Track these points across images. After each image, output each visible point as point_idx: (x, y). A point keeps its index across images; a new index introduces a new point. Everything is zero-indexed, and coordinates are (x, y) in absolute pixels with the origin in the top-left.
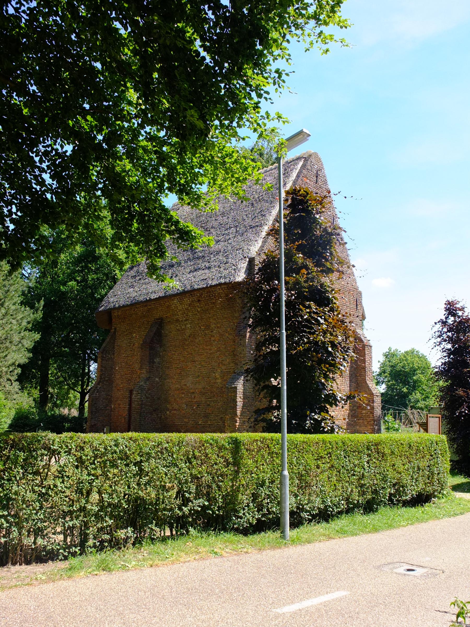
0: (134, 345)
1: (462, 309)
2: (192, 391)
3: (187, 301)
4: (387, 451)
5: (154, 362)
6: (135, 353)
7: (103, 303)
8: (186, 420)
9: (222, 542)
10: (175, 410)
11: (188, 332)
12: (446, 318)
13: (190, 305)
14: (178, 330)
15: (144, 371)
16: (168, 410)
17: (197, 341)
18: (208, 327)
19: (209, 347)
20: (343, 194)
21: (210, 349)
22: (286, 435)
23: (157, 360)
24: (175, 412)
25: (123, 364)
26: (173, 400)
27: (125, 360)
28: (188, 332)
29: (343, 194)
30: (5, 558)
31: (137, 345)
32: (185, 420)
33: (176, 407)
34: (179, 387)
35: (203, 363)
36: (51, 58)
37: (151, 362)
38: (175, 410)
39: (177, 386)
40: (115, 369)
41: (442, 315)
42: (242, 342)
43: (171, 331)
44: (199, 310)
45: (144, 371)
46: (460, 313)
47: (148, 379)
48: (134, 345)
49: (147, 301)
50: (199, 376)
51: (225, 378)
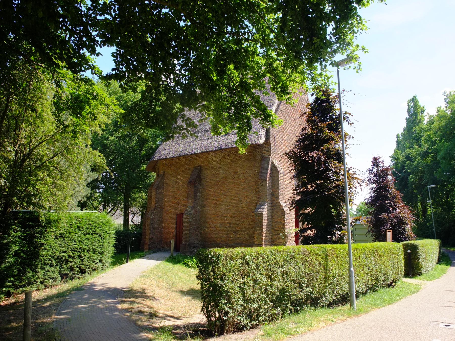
0: (179, 184)
1: (383, 162)
2: (225, 215)
3: (220, 155)
4: (382, 254)
5: (197, 196)
6: (180, 189)
7: (157, 154)
8: (221, 235)
9: (322, 314)
10: (212, 228)
11: (221, 176)
12: (372, 168)
13: (222, 158)
14: (213, 174)
15: (190, 201)
16: (207, 228)
17: (228, 182)
18: (236, 173)
19: (237, 186)
20: (353, 92)
21: (238, 188)
22: (352, 245)
23: (198, 194)
24: (212, 229)
25: (171, 196)
26: (210, 221)
27: (173, 194)
28: (221, 176)
29: (353, 92)
30: (178, 331)
31: (181, 183)
32: (220, 235)
33: (212, 225)
34: (215, 213)
35: (213, 196)
36: (224, 3)
37: (195, 196)
38: (212, 228)
39: (213, 212)
40: (164, 200)
41: (369, 165)
42: (264, 183)
43: (207, 174)
44: (229, 161)
45: (190, 201)
46: (382, 165)
47: (193, 207)
48: (179, 184)
49: (192, 154)
50: (230, 205)
51: (249, 207)
